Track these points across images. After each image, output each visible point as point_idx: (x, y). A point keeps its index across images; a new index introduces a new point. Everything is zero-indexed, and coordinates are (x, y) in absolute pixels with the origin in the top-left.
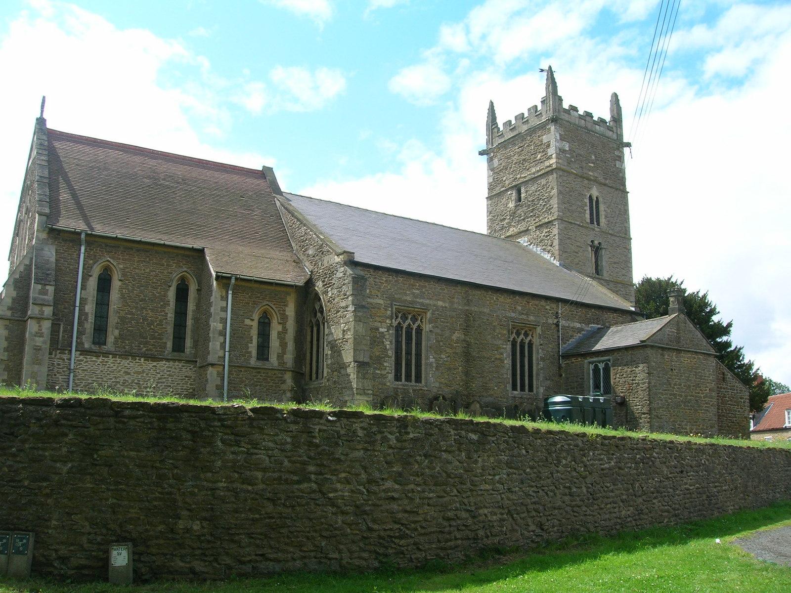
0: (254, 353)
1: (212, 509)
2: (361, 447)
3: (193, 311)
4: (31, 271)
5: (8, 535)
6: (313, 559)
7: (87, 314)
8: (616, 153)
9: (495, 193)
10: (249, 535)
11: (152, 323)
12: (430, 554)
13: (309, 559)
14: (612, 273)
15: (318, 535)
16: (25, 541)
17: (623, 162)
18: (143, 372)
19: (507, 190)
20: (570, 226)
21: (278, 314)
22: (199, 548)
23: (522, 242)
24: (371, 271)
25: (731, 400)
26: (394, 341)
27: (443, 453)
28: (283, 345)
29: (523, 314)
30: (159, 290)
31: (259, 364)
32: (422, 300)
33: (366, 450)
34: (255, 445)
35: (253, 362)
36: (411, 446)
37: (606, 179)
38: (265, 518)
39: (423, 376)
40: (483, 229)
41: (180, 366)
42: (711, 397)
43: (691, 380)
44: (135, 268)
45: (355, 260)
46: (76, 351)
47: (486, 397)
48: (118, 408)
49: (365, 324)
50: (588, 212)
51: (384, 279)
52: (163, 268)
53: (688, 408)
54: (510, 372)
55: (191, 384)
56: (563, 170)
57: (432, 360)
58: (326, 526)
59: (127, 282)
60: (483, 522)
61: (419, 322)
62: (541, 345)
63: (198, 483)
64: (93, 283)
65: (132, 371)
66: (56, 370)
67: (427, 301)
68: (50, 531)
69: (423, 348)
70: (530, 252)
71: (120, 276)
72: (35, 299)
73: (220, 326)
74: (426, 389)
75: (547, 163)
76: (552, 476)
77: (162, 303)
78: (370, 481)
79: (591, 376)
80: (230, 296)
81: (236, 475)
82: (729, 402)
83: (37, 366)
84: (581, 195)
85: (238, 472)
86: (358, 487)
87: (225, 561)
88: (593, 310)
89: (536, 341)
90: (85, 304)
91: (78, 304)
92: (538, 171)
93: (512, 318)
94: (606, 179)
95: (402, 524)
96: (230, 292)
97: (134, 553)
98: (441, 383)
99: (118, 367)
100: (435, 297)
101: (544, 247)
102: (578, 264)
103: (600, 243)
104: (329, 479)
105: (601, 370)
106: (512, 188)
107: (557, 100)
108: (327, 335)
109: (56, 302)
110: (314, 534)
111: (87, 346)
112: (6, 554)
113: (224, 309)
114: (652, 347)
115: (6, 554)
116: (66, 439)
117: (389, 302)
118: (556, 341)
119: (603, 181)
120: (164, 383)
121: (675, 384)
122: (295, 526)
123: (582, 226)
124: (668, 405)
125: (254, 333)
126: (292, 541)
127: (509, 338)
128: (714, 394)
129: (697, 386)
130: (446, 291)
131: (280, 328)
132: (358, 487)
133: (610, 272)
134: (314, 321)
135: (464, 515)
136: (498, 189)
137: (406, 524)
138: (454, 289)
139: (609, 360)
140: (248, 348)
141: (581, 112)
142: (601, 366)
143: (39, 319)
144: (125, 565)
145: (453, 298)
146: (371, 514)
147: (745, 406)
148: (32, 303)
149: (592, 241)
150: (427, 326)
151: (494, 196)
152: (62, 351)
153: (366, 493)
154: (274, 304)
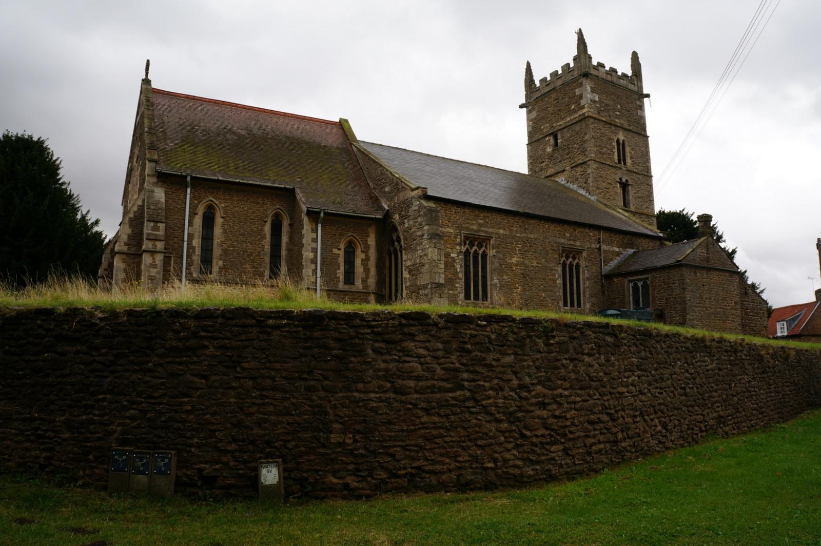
0: (342, 278)
1: (365, 421)
2: (511, 352)
4: (144, 211)
5: (149, 454)
6: (469, 470)
7: (194, 248)
9: (534, 140)
10: (404, 448)
11: (251, 254)
12: (577, 459)
13: (465, 469)
15: (473, 444)
16: (166, 460)
17: (644, 111)
19: (545, 137)
20: (602, 166)
22: (352, 463)
23: (559, 181)
24: (442, 204)
25: (752, 312)
26: (463, 265)
27: (585, 357)
28: (367, 270)
29: (570, 240)
30: (256, 226)
31: (346, 288)
33: (515, 354)
34: (406, 352)
35: (341, 286)
36: (557, 350)
37: (630, 126)
38: (420, 429)
39: (489, 295)
42: (736, 309)
43: (719, 295)
44: (234, 207)
48: (261, 317)
50: (616, 154)
52: (259, 206)
54: (561, 291)
56: (595, 118)
57: (496, 281)
58: (481, 435)
60: (622, 424)
62: (587, 267)
63: (349, 394)
64: (198, 220)
67: (491, 230)
68: (193, 450)
70: (568, 188)
71: (222, 213)
72: (148, 234)
73: (311, 255)
75: (580, 113)
76: (671, 377)
77: (259, 237)
78: (522, 387)
80: (319, 229)
81: (389, 385)
82: (751, 314)
84: (610, 139)
85: (389, 381)
86: (511, 393)
87: (380, 475)
89: (583, 264)
90: (192, 239)
91: (186, 239)
92: (572, 120)
93: (562, 243)
94: (630, 126)
95: (552, 430)
97: (285, 470)
101: (580, 184)
102: (609, 198)
103: (627, 181)
104: (483, 385)
105: (640, 287)
107: (587, 58)
108: (405, 261)
109: (167, 238)
110: (468, 443)
111: (195, 275)
112: (147, 474)
114: (687, 266)
115: (147, 474)
116: (207, 352)
117: (458, 231)
121: (706, 299)
122: (451, 436)
123: (612, 166)
125: (341, 260)
126: (448, 452)
127: (560, 261)
128: (738, 306)
129: (724, 299)
131: (363, 256)
132: (511, 393)
133: (636, 205)
134: (392, 249)
135: (605, 418)
136: (536, 136)
137: (556, 430)
139: (647, 278)
140: (336, 274)
141: (607, 68)
142: (640, 284)
144: (276, 483)
145: (512, 227)
146: (524, 420)
147: (763, 316)
148: (147, 239)
149: (621, 179)
150: (491, 251)
151: (534, 141)
153: (517, 399)
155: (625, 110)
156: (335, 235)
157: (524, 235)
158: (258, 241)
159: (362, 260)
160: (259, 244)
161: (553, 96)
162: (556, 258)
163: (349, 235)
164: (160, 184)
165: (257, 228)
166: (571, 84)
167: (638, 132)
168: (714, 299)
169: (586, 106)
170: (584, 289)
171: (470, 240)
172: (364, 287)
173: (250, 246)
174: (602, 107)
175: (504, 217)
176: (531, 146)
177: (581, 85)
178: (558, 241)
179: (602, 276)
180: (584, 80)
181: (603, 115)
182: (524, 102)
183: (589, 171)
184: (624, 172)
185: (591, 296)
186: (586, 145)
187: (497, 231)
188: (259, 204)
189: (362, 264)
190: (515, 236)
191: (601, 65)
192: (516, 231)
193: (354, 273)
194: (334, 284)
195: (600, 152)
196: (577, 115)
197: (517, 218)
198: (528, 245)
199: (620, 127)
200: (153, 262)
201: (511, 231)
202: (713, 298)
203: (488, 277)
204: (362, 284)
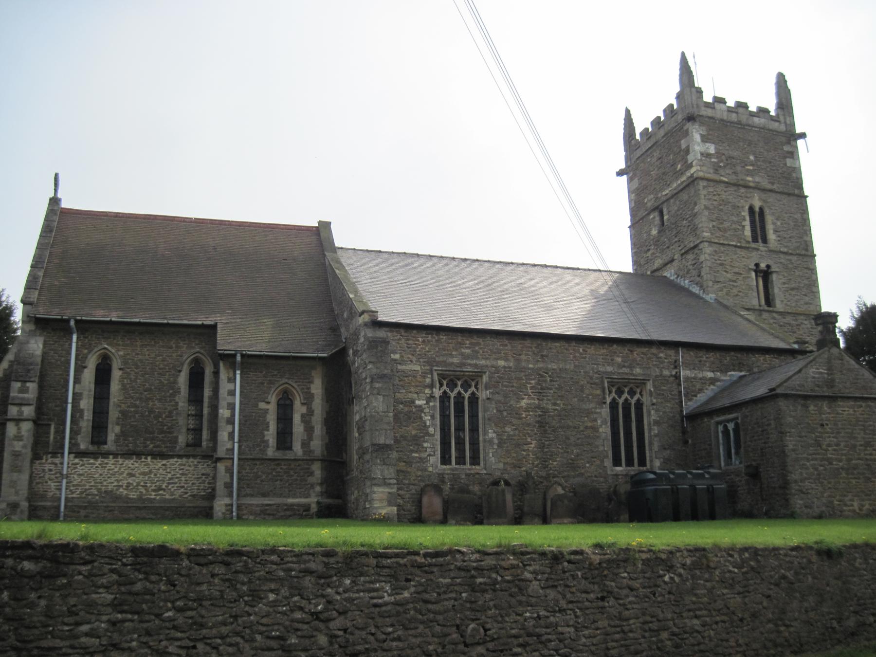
3: (210, 398)
7: (82, 411)
8: (786, 148)
11: (159, 415)
14: (789, 303)
18: (150, 472)
19: (649, 214)
20: (722, 249)
21: (300, 392)
23: (668, 275)
29: (624, 366)
30: (167, 377)
32: (474, 362)
35: (271, 452)
37: (773, 184)
40: (631, 271)
41: (195, 463)
44: (137, 354)
45: (380, 319)
46: (69, 453)
47: (574, 478)
49: (386, 397)
51: (420, 339)
52: (171, 350)
53: (853, 476)
55: (209, 483)
56: (708, 180)
57: (491, 434)
59: (128, 370)
61: (473, 389)
62: (653, 404)
64: (89, 376)
65: (136, 472)
66: (47, 476)
69: (480, 421)
71: (120, 364)
74: (485, 472)
75: (688, 174)
77: (171, 391)
79: (721, 441)
80: (238, 377)
83: (16, 474)
84: (735, 207)
88: (733, 353)
91: (70, 400)
92: (679, 185)
93: (606, 373)
94: (773, 184)
96: (238, 372)
98: (505, 464)
99: (120, 469)
100: (494, 356)
101: (692, 279)
102: (737, 295)
103: (768, 266)
105: (731, 432)
106: (654, 210)
113: (232, 393)
114: (786, 396)
117: (428, 368)
118: (677, 397)
119: (769, 187)
120: (176, 483)
121: (829, 445)
124: (819, 474)
125: (272, 419)
130: (509, 347)
131: (304, 409)
138: (520, 344)
141: (731, 103)
142: (731, 426)
143: (18, 421)
145: (520, 355)
152: (54, 454)
154: (296, 382)
155: (763, 161)
156: (263, 383)
157: (541, 365)
158: (170, 397)
159: (303, 416)
160: (171, 401)
161: (656, 154)
162: (599, 395)
163: (281, 382)
164: (38, 332)
165: (168, 380)
166: (675, 134)
167: (786, 191)
168: (846, 446)
169: (694, 163)
170: (650, 437)
171: (450, 379)
172: (305, 453)
173: (158, 404)
174: (722, 161)
175: (507, 342)
176: (634, 228)
177: (687, 134)
178: (601, 369)
179: (683, 417)
180: (689, 125)
181: (723, 174)
182: (623, 166)
183: (702, 258)
184: (763, 253)
185: (663, 448)
186: (696, 221)
187: (494, 363)
188: (171, 348)
189: (302, 421)
190: (524, 368)
191: (720, 101)
192: (528, 361)
193: (291, 433)
194: (260, 450)
195: (719, 228)
196: (684, 178)
197: (529, 341)
198: (548, 379)
199: (754, 188)
200: (19, 433)
201: (518, 361)
202: (842, 444)
203: (480, 430)
204: (302, 447)
